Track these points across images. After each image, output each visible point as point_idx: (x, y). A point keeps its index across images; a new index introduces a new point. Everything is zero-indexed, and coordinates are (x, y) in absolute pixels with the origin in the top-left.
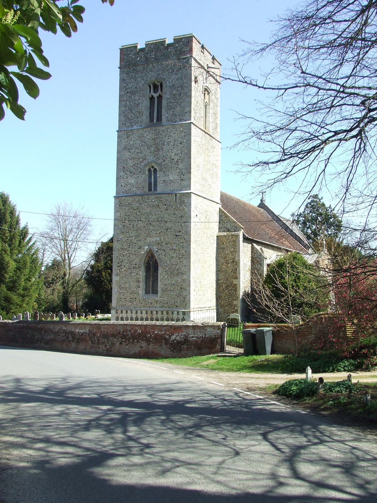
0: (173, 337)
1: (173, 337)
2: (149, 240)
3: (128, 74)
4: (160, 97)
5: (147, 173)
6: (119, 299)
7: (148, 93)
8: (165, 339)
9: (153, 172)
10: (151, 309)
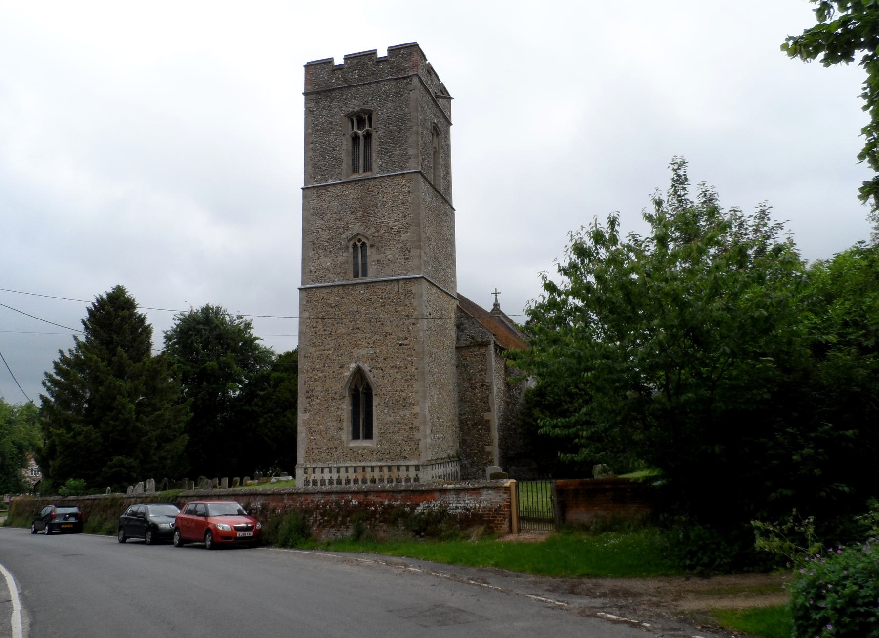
0: (419, 510)
1: (419, 510)
2: (356, 352)
4: (368, 136)
5: (351, 250)
6: (309, 452)
7: (349, 130)
8: (404, 515)
9: (359, 246)
10: (363, 464)
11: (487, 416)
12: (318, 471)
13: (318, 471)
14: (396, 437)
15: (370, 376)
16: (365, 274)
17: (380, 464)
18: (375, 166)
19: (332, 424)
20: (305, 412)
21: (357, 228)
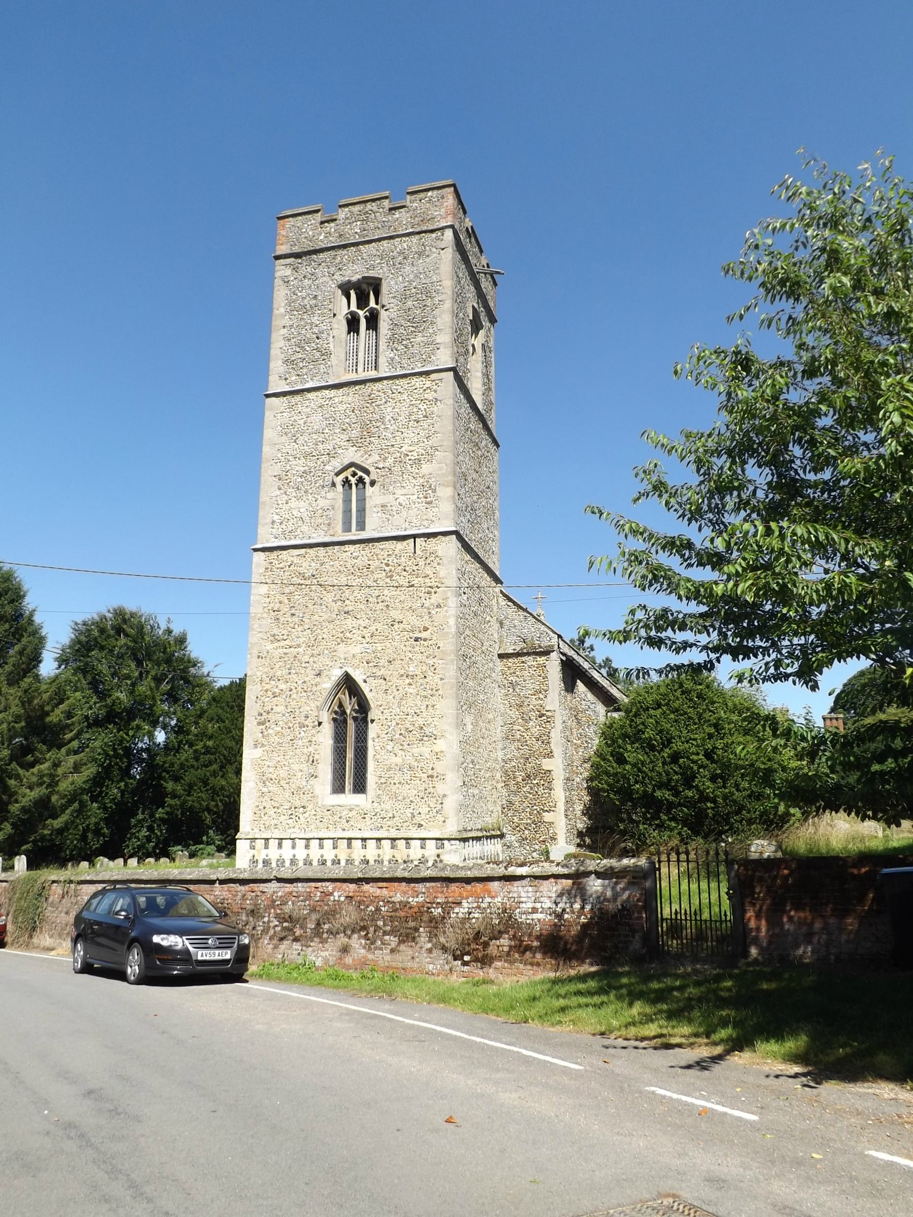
3: (295, 269)
6: (259, 812)
11: (546, 764)
12: (273, 844)
13: (273, 844)
14: (404, 790)
15: (365, 688)
16: (361, 526)
17: (393, 834)
18: (382, 360)
19: (299, 767)
20: (256, 746)
21: (351, 455)
